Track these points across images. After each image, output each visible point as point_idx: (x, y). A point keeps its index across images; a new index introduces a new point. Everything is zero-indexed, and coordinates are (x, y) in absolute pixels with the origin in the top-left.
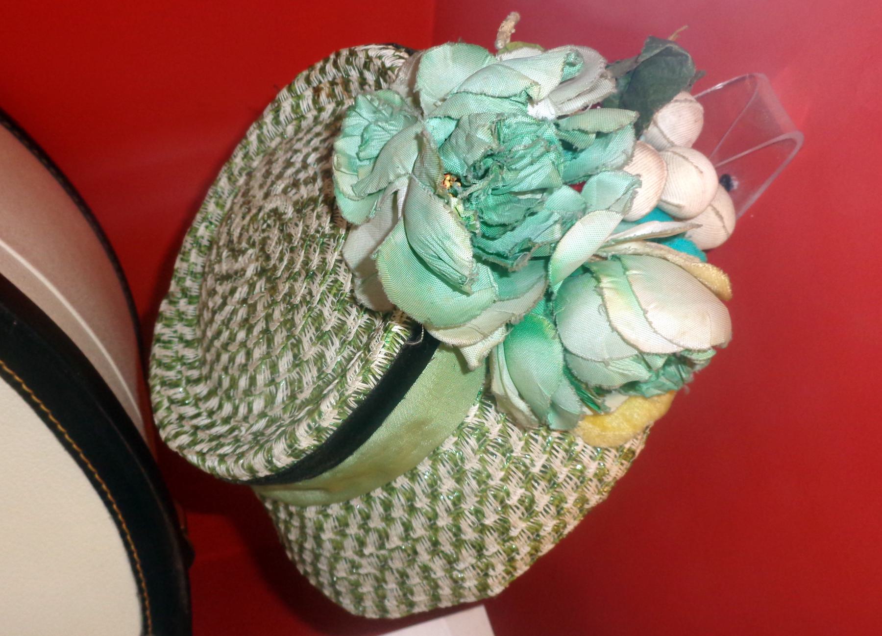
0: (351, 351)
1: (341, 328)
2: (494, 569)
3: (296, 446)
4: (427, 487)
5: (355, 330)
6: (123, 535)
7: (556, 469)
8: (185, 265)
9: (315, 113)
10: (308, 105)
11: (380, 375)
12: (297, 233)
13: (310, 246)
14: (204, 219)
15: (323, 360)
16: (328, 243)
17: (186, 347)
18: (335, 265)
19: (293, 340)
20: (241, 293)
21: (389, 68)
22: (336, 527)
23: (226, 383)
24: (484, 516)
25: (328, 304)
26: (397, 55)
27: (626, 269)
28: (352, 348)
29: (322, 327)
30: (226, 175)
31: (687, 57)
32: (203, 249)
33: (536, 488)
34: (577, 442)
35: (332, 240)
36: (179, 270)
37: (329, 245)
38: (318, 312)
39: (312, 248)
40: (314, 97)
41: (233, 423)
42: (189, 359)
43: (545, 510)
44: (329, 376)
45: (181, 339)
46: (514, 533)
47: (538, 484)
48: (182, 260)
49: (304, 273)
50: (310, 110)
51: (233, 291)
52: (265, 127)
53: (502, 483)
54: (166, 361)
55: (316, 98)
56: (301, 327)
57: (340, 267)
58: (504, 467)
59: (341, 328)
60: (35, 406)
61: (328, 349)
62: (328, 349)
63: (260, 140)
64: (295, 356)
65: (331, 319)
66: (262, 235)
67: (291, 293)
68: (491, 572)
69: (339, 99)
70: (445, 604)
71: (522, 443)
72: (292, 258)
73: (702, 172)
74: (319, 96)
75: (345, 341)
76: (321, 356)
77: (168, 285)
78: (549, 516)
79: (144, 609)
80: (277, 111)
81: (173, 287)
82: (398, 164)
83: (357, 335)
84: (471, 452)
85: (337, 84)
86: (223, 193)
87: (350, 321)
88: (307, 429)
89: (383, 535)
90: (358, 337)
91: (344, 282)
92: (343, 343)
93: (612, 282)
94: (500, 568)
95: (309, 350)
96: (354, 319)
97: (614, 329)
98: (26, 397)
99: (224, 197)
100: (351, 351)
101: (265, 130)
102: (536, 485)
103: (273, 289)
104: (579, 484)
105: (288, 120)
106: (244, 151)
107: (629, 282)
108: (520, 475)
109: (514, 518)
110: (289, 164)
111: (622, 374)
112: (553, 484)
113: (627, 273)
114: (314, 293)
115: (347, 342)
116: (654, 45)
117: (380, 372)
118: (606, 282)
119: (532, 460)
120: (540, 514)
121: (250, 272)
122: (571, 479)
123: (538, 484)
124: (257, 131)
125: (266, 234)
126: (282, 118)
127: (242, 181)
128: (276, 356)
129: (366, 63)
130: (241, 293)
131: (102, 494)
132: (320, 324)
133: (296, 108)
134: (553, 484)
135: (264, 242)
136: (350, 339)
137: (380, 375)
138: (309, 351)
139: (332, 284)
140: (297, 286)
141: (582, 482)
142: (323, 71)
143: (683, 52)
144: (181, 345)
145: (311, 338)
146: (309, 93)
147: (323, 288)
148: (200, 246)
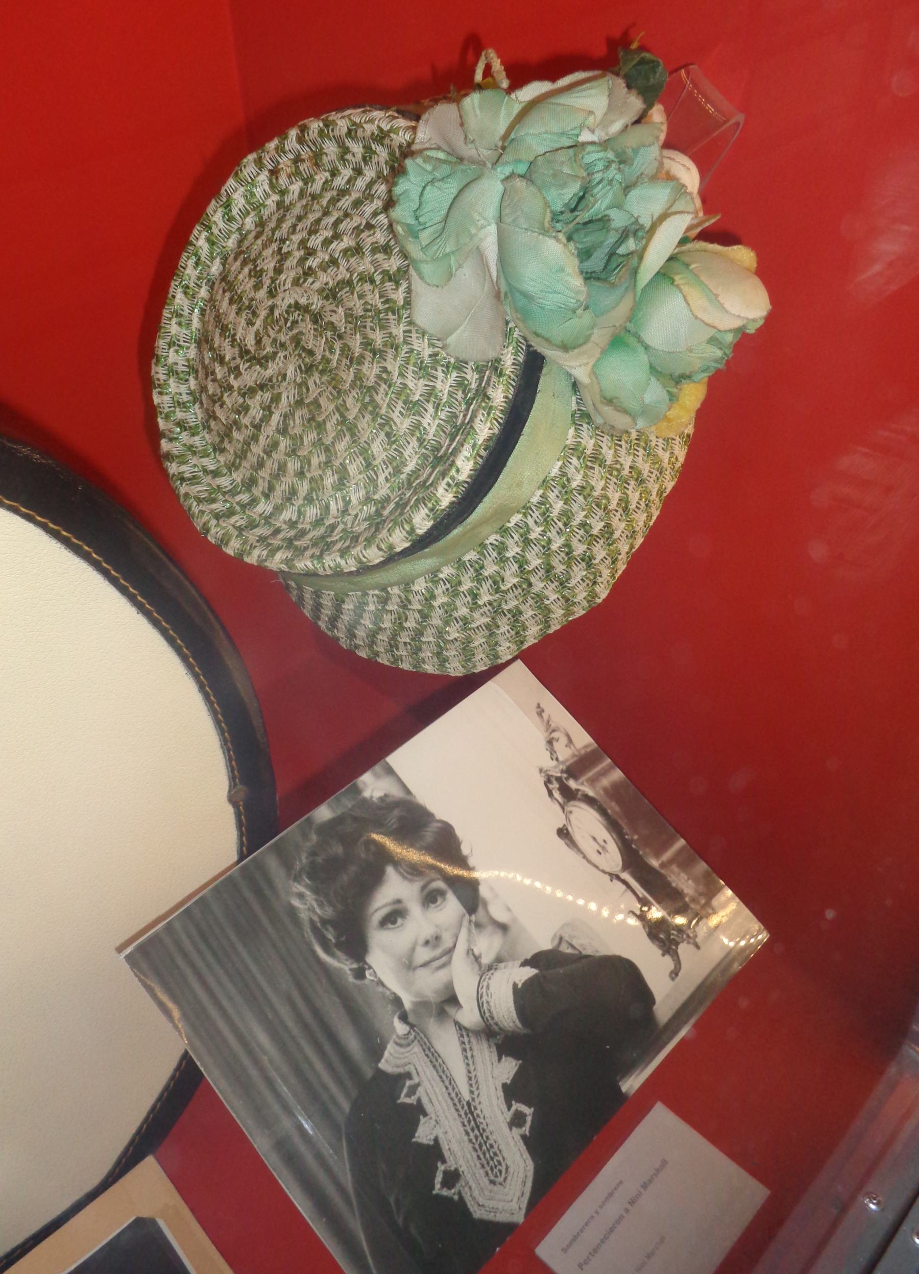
0: (448, 412)
1: (431, 393)
2: (601, 576)
3: (438, 507)
4: (539, 517)
5: (447, 390)
6: (202, 688)
7: (641, 467)
8: (166, 398)
9: (276, 198)
10: (264, 191)
11: (501, 418)
12: (338, 318)
13: (365, 327)
14: (170, 345)
15: (421, 428)
16: (387, 317)
17: (213, 478)
18: (405, 337)
19: (380, 421)
20: (288, 397)
21: (389, 131)
22: (447, 590)
23: (303, 488)
24: (591, 528)
25: (410, 375)
26: (388, 116)
27: (687, 265)
28: (448, 409)
29: (410, 399)
30: (180, 290)
31: (658, 63)
32: (182, 376)
33: (628, 489)
34: (650, 438)
35: (390, 314)
36: (161, 405)
37: (388, 319)
38: (401, 386)
39: (368, 328)
40: (270, 180)
41: (329, 521)
42: (226, 487)
43: (637, 507)
44: (431, 442)
45: (205, 471)
46: (617, 535)
47: (629, 484)
48: (161, 393)
49: (368, 355)
50: (267, 195)
51: (276, 399)
52: (214, 227)
53: (603, 492)
54: (204, 495)
55: (274, 181)
56: (385, 405)
57: (411, 337)
58: (602, 476)
59: (431, 393)
60: (105, 573)
61: (423, 417)
62: (423, 417)
63: (212, 243)
64: (388, 435)
65: (417, 387)
66: (290, 334)
67: (358, 377)
68: (599, 580)
69: (306, 177)
70: (481, 668)
71: (612, 451)
72: (345, 345)
73: (689, 169)
74: (277, 178)
75: (439, 404)
76: (417, 426)
77: (156, 425)
78: (640, 511)
79: (229, 760)
80: (227, 206)
81: (162, 423)
82: (477, 217)
83: (450, 394)
84: (575, 471)
85: (303, 161)
86: (182, 310)
87: (439, 385)
88: (446, 487)
89: (498, 579)
90: (452, 397)
91: (420, 349)
92: (437, 407)
93: (683, 278)
94: (606, 573)
95: (402, 423)
96: (442, 381)
97: (696, 318)
98: (96, 565)
99: (186, 312)
100: (448, 412)
101: (215, 231)
102: (627, 486)
103: (335, 382)
104: (658, 475)
105: (241, 212)
106: (194, 259)
107: (696, 275)
108: (614, 480)
109: (615, 522)
110: (283, 257)
111: (701, 358)
112: (640, 481)
113: (691, 268)
114: (389, 369)
115: (442, 405)
116: (629, 57)
117: (501, 416)
118: (677, 278)
119: (621, 465)
120: (462, 594)
121: (290, 371)
122: (652, 473)
123: (629, 484)
124: (205, 234)
125: (295, 331)
126: (235, 212)
127: (203, 293)
128: (365, 442)
129: (350, 131)
130: (288, 397)
131: (178, 650)
132: (408, 396)
133: (249, 196)
134: (640, 481)
135: (297, 341)
136: (444, 401)
137: (501, 418)
138: (403, 424)
139: (408, 355)
140: (365, 369)
141: (660, 473)
142: (281, 150)
143: (655, 59)
144: (210, 477)
145: (400, 412)
146: (264, 177)
147: (399, 361)
148: (177, 374)
